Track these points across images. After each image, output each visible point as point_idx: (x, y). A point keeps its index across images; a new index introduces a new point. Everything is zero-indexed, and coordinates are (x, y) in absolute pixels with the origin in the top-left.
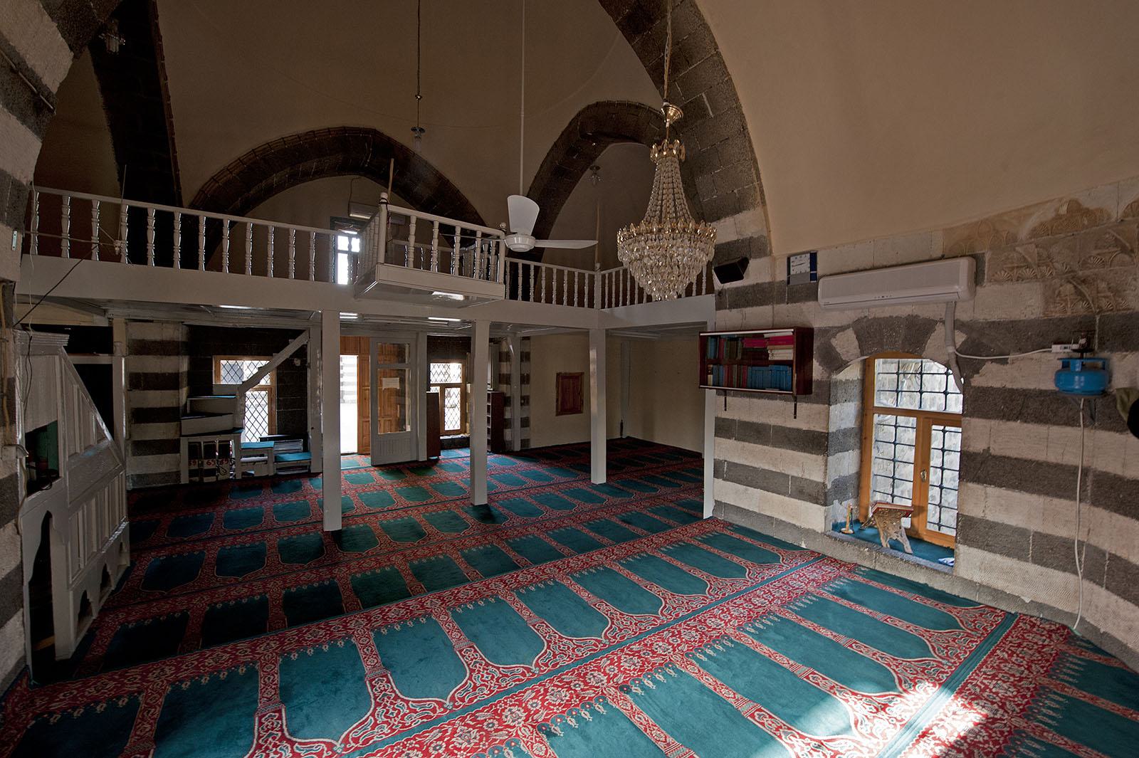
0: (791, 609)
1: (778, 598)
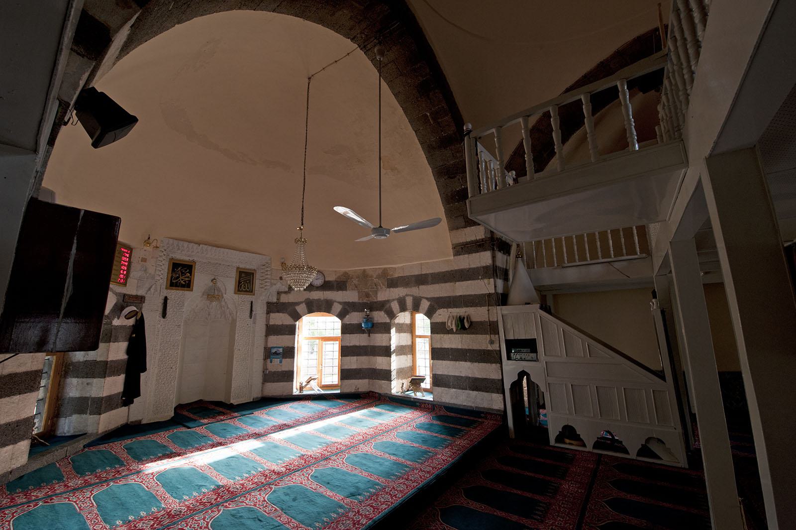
0: (409, 468)
1: (416, 474)
